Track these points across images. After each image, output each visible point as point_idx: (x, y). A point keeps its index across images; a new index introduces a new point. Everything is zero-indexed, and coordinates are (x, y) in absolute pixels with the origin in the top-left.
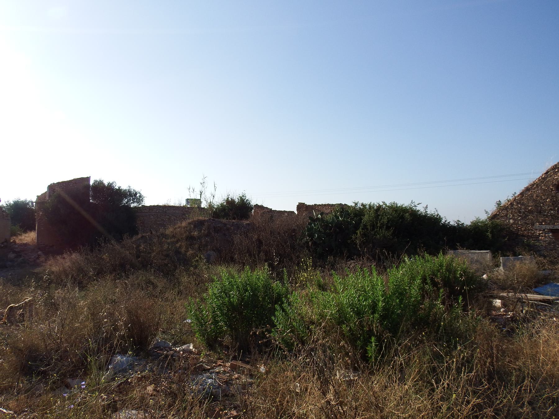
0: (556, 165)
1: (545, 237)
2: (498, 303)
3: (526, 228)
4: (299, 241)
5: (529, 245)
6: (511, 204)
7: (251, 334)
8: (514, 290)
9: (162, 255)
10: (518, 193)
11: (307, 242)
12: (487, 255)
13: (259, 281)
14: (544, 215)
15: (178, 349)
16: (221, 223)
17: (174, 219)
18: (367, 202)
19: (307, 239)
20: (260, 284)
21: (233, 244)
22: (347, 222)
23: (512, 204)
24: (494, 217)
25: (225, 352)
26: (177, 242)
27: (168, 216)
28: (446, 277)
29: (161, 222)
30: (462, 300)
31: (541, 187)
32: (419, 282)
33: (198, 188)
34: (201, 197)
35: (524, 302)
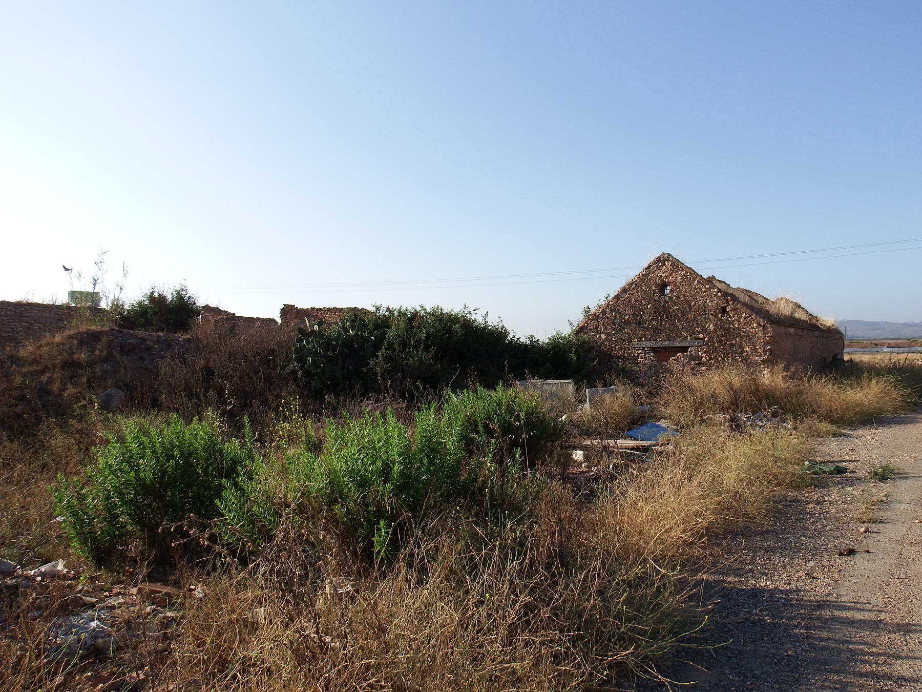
0: (660, 257)
1: (645, 358)
2: (578, 455)
3: (621, 346)
4: (281, 369)
5: (624, 371)
6: (603, 311)
7: (159, 531)
8: (600, 434)
9: (10, 397)
10: (612, 296)
11: (294, 372)
12: (568, 386)
13: (196, 439)
14: (644, 328)
15: (32, 573)
16: (136, 337)
17: (40, 329)
18: (395, 306)
19: (294, 366)
20: (199, 445)
21: (158, 376)
22: (362, 337)
23: (604, 312)
24: (581, 330)
25: (129, 569)
26: (43, 371)
27: (27, 322)
28: (505, 420)
29: (10, 334)
30: (520, 455)
31: (641, 288)
32: (459, 430)
33: (90, 272)
34: (94, 288)
35: (613, 452)
